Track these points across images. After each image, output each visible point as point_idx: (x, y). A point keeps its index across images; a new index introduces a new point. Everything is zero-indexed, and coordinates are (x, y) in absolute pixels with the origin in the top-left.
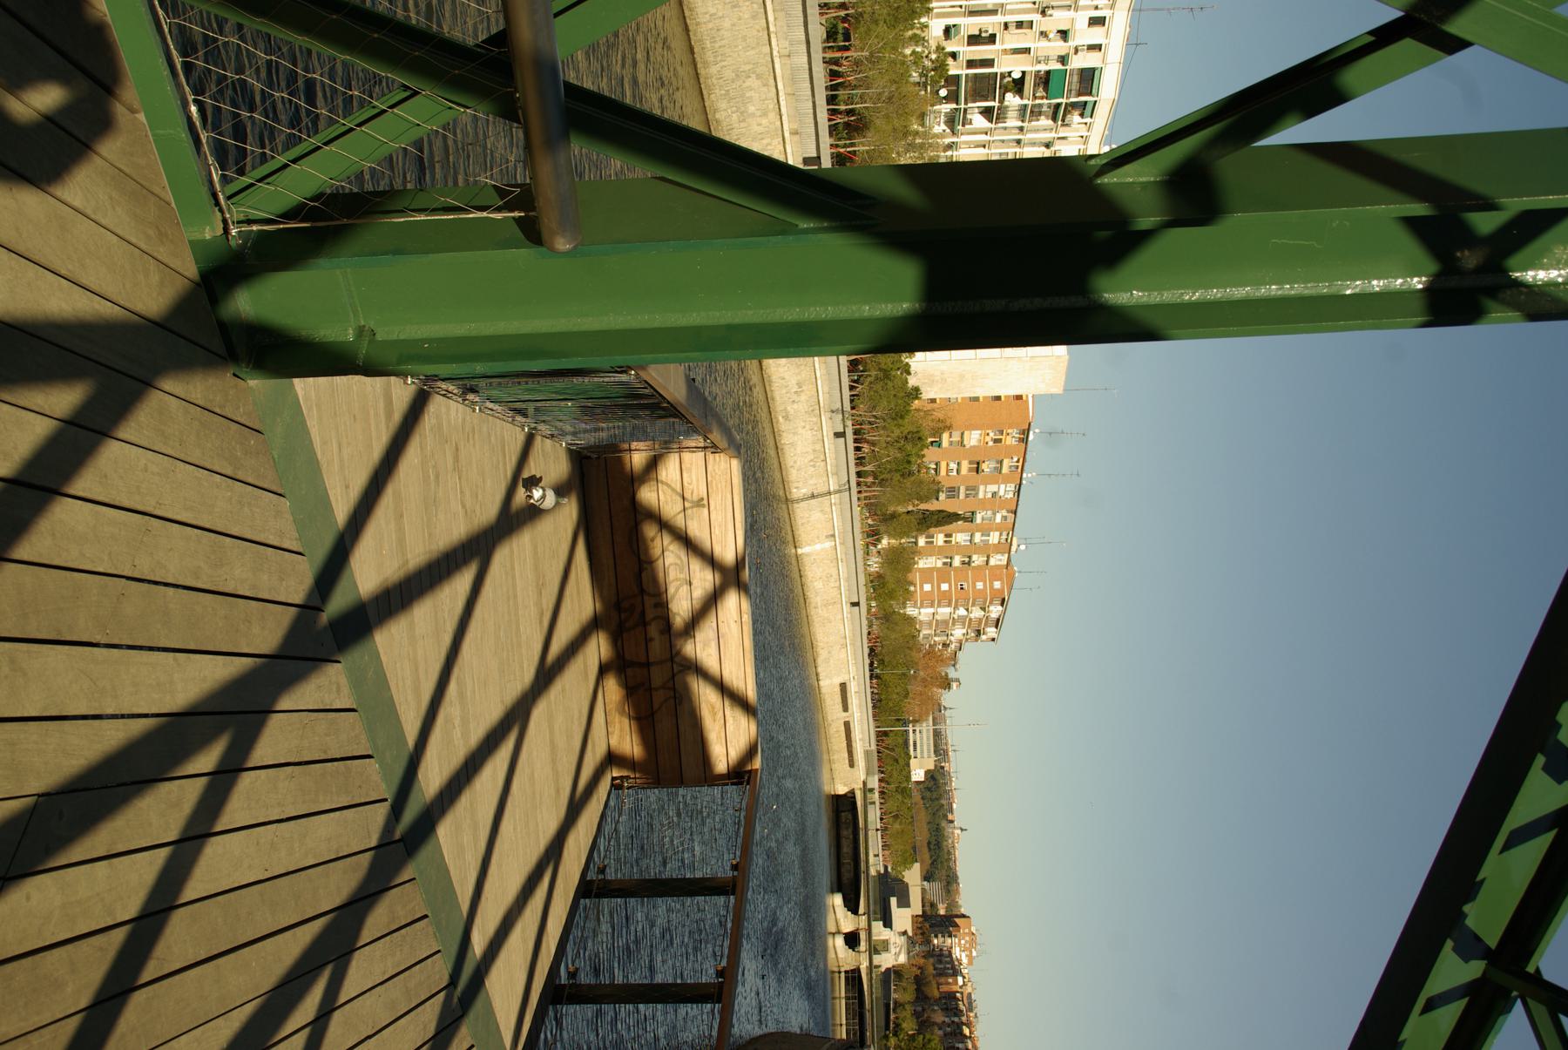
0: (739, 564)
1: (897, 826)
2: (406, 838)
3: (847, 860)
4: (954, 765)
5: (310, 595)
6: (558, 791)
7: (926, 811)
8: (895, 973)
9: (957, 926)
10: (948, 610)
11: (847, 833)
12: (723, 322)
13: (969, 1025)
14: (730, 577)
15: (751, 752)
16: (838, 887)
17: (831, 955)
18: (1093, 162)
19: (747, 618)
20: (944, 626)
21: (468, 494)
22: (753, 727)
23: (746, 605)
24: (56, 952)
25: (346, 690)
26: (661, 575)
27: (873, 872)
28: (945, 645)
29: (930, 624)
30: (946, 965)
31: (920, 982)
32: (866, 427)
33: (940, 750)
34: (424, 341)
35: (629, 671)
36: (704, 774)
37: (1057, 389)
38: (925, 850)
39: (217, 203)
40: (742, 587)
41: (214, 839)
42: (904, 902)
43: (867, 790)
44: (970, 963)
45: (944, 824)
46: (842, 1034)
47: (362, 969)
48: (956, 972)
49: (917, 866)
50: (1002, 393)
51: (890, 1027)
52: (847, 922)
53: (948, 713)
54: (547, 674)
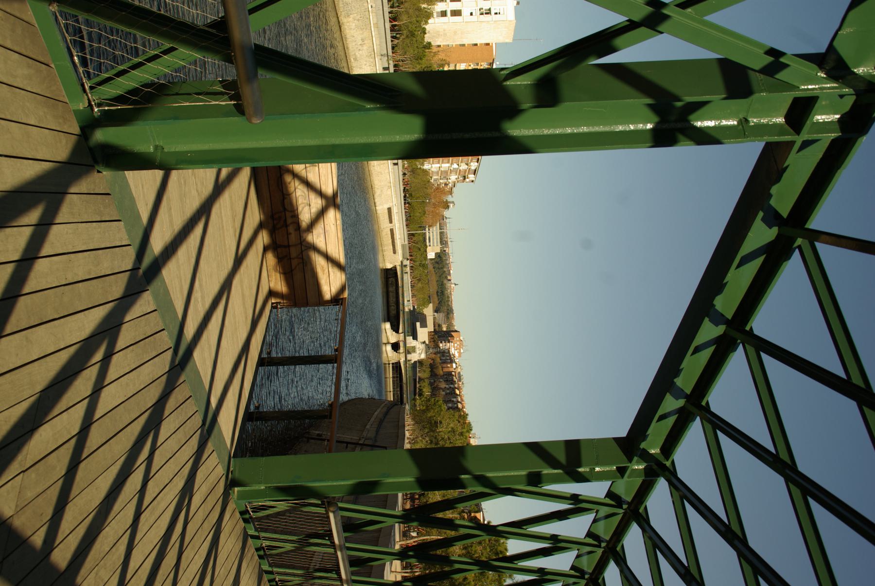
0: (335, 195)
1: (420, 285)
2: (181, 360)
3: (392, 300)
4: (450, 250)
5: (135, 264)
6: (246, 318)
7: (435, 275)
8: (420, 362)
9: (452, 336)
10: (448, 165)
11: (392, 289)
12: (330, 143)
13: (459, 389)
14: (331, 202)
15: (342, 289)
16: (388, 319)
17: (384, 355)
18: (502, 72)
19: (339, 222)
20: (445, 174)
21: (199, 184)
22: (344, 277)
23: (339, 216)
24: (52, 455)
25: (152, 302)
26: (294, 201)
27: (407, 310)
28: (446, 184)
29: (437, 173)
30: (446, 357)
31: (432, 367)
32: (400, 63)
33: (443, 241)
34: (188, 152)
35: (279, 250)
36: (319, 301)
37: (509, 40)
38: (435, 296)
39: (84, 91)
40: (336, 206)
41: (104, 389)
42: (424, 325)
43: (403, 266)
44: (460, 356)
45: (445, 281)
46: (391, 398)
47: (166, 429)
48: (452, 361)
49: (431, 305)
50: (478, 42)
51: (417, 392)
52: (393, 337)
53: (448, 221)
54: (239, 260)
